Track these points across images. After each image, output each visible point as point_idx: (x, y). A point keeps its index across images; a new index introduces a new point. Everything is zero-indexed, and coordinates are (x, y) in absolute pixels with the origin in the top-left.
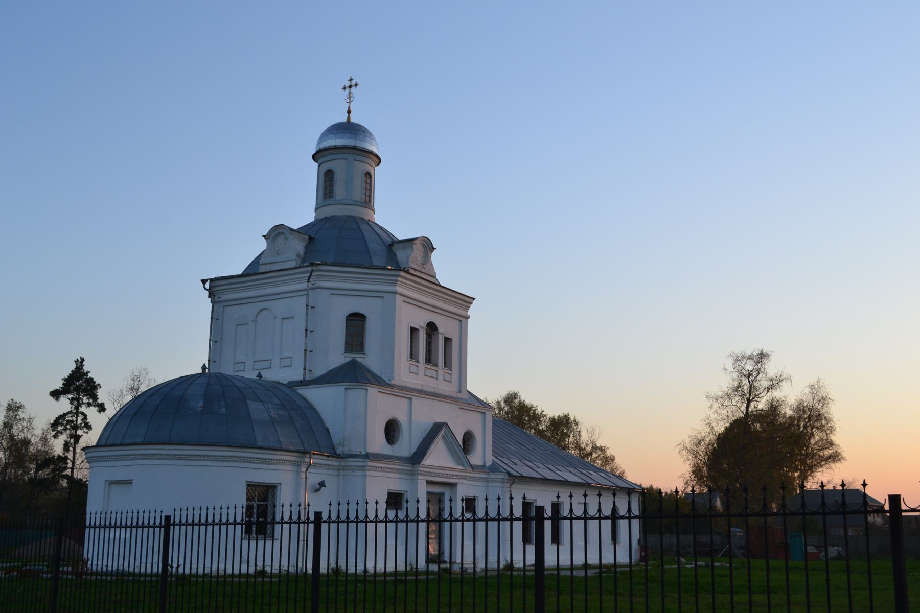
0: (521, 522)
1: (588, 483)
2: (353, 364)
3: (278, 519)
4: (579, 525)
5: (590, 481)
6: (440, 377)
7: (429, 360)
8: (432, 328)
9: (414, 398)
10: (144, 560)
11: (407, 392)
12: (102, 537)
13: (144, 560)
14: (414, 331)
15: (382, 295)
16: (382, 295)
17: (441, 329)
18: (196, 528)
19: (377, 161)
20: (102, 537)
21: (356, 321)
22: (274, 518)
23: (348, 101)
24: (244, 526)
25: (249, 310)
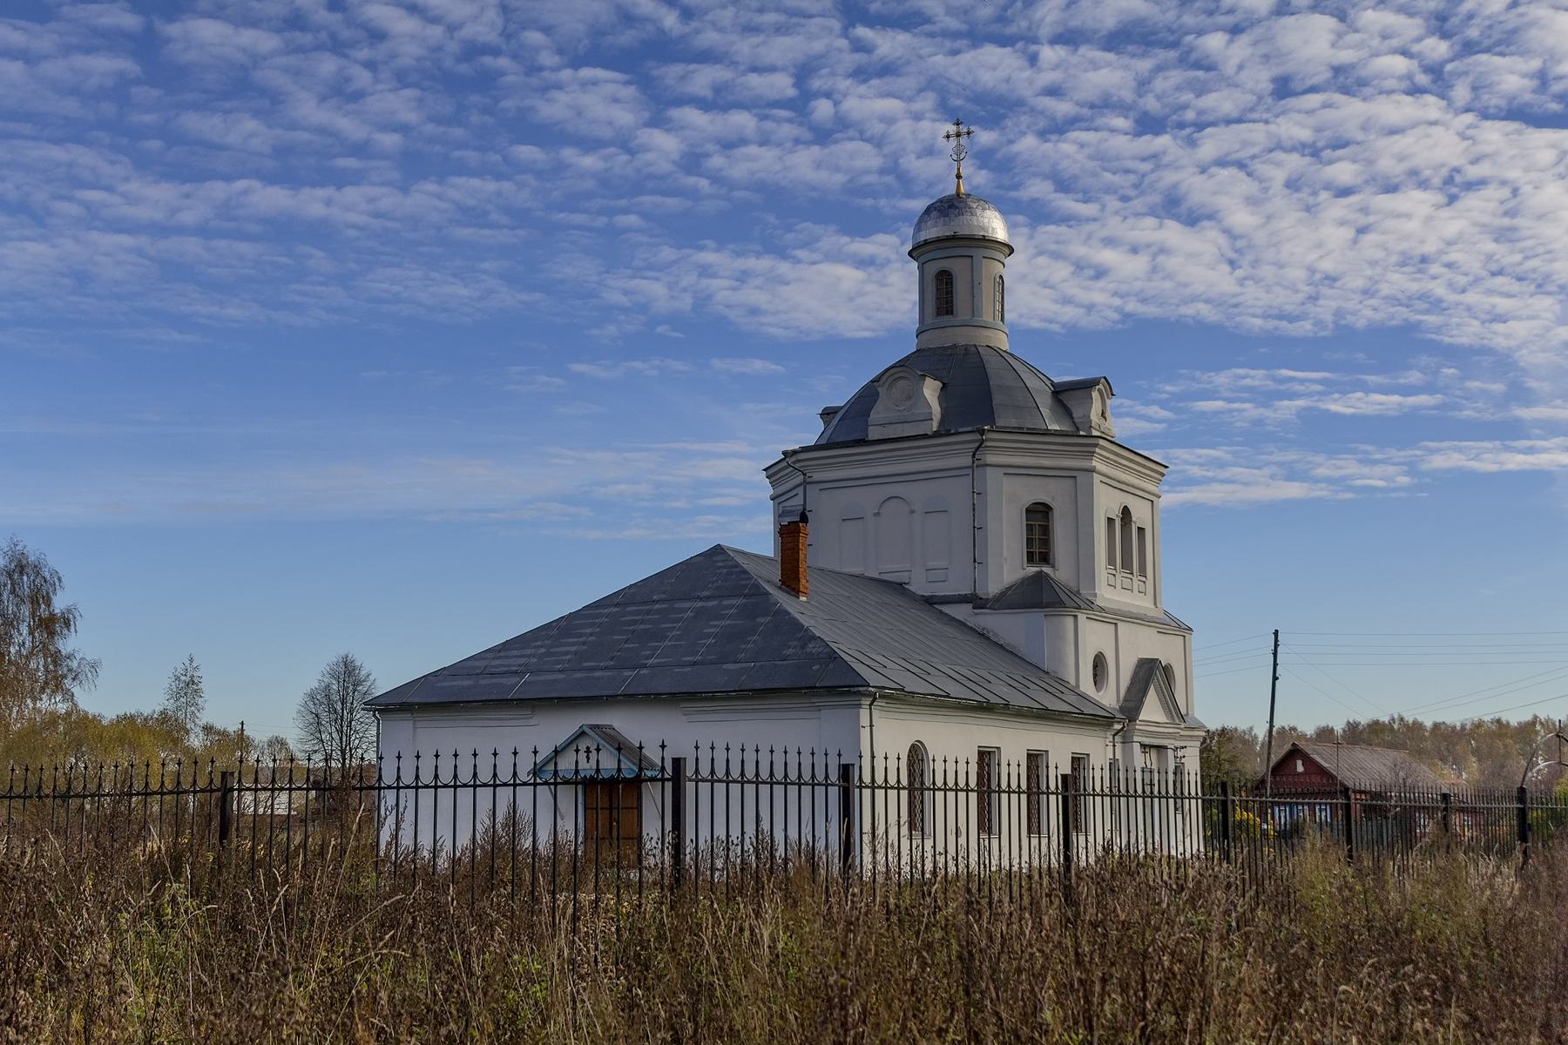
0: (976, 794)
1: (988, 702)
2: (1040, 578)
3: (928, 783)
4: (940, 795)
5: (994, 700)
6: (1119, 586)
7: (1127, 564)
8: (1126, 511)
9: (1120, 624)
10: (1141, 834)
11: (1114, 618)
12: (792, 808)
13: (1141, 834)
14: (1110, 521)
15: (1074, 473)
16: (1074, 473)
17: (1135, 516)
18: (445, 796)
19: (1007, 251)
20: (792, 808)
21: (1039, 514)
22: (922, 783)
23: (955, 157)
24: (1060, 797)
25: (868, 498)
